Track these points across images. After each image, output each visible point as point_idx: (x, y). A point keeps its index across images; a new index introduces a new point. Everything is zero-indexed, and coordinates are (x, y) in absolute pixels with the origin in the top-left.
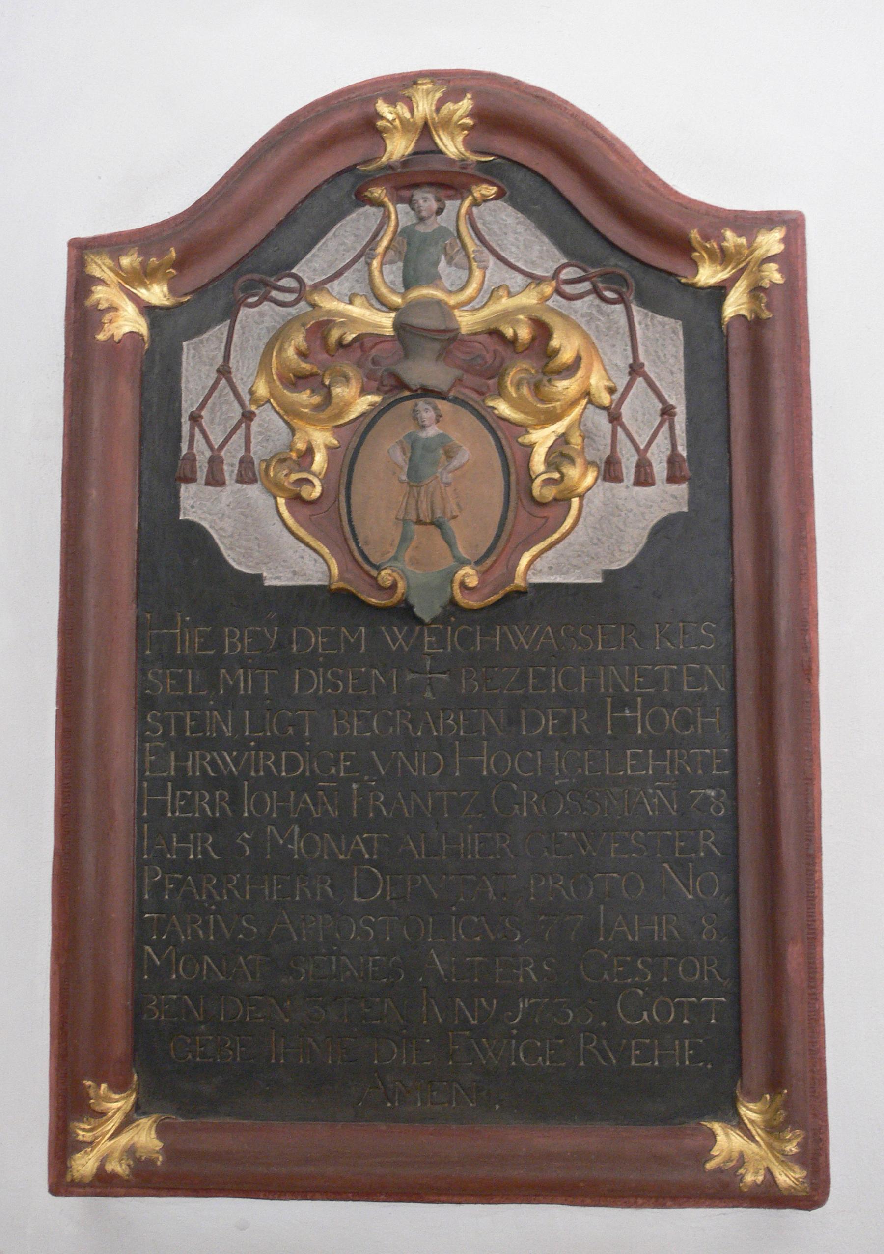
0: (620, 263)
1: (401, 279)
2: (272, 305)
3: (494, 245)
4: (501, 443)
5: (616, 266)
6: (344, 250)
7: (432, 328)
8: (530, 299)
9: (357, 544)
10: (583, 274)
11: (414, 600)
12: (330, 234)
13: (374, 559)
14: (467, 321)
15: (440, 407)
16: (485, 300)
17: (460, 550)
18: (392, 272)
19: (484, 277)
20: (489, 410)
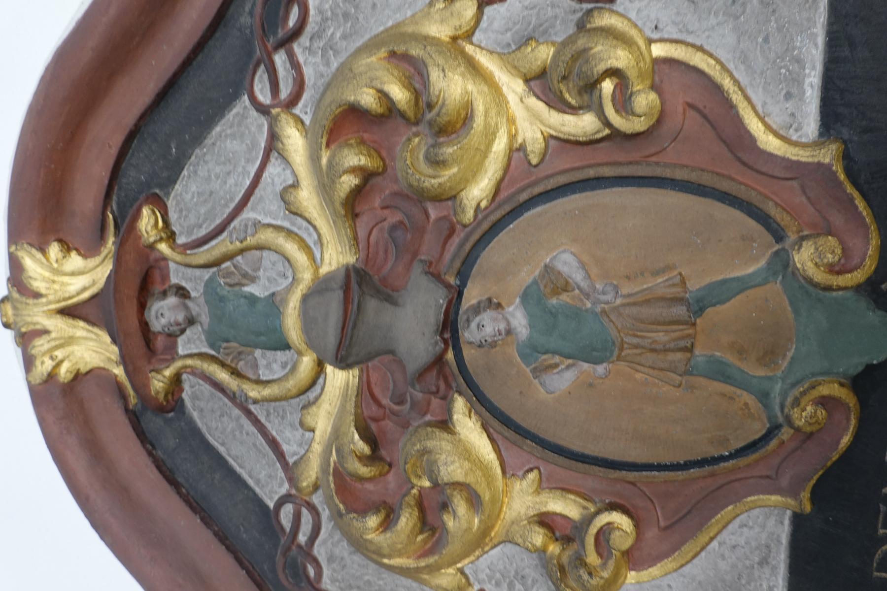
0: (247, 9)
1: (279, 353)
2: (317, 542)
3: (228, 211)
4: (540, 194)
5: (251, 13)
6: (241, 432)
7: (341, 313)
8: (295, 141)
9: (723, 459)
10: (262, 67)
11: (855, 364)
12: (222, 450)
13: (757, 430)
14: (336, 256)
15: (474, 302)
16: (305, 224)
17: (751, 270)
18: (268, 366)
19: (269, 226)
20: (480, 216)
